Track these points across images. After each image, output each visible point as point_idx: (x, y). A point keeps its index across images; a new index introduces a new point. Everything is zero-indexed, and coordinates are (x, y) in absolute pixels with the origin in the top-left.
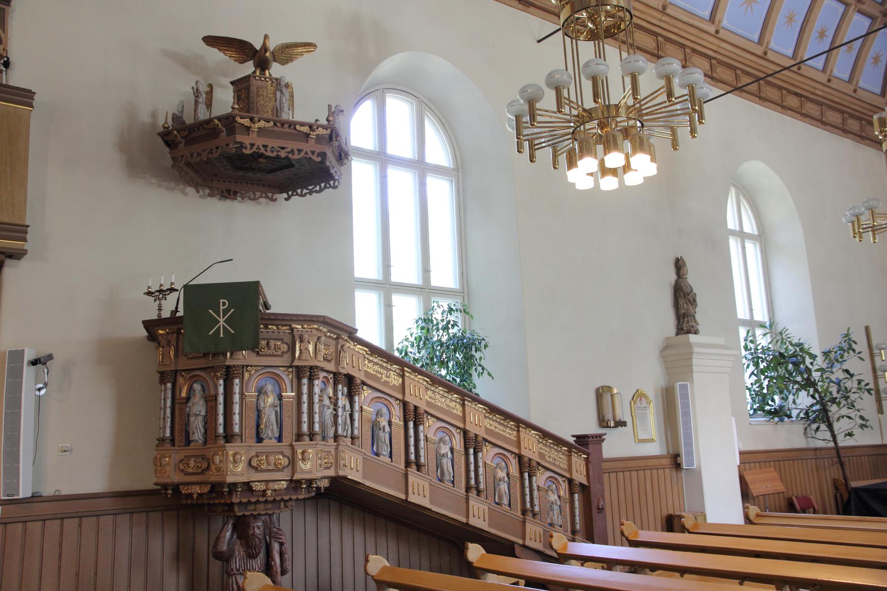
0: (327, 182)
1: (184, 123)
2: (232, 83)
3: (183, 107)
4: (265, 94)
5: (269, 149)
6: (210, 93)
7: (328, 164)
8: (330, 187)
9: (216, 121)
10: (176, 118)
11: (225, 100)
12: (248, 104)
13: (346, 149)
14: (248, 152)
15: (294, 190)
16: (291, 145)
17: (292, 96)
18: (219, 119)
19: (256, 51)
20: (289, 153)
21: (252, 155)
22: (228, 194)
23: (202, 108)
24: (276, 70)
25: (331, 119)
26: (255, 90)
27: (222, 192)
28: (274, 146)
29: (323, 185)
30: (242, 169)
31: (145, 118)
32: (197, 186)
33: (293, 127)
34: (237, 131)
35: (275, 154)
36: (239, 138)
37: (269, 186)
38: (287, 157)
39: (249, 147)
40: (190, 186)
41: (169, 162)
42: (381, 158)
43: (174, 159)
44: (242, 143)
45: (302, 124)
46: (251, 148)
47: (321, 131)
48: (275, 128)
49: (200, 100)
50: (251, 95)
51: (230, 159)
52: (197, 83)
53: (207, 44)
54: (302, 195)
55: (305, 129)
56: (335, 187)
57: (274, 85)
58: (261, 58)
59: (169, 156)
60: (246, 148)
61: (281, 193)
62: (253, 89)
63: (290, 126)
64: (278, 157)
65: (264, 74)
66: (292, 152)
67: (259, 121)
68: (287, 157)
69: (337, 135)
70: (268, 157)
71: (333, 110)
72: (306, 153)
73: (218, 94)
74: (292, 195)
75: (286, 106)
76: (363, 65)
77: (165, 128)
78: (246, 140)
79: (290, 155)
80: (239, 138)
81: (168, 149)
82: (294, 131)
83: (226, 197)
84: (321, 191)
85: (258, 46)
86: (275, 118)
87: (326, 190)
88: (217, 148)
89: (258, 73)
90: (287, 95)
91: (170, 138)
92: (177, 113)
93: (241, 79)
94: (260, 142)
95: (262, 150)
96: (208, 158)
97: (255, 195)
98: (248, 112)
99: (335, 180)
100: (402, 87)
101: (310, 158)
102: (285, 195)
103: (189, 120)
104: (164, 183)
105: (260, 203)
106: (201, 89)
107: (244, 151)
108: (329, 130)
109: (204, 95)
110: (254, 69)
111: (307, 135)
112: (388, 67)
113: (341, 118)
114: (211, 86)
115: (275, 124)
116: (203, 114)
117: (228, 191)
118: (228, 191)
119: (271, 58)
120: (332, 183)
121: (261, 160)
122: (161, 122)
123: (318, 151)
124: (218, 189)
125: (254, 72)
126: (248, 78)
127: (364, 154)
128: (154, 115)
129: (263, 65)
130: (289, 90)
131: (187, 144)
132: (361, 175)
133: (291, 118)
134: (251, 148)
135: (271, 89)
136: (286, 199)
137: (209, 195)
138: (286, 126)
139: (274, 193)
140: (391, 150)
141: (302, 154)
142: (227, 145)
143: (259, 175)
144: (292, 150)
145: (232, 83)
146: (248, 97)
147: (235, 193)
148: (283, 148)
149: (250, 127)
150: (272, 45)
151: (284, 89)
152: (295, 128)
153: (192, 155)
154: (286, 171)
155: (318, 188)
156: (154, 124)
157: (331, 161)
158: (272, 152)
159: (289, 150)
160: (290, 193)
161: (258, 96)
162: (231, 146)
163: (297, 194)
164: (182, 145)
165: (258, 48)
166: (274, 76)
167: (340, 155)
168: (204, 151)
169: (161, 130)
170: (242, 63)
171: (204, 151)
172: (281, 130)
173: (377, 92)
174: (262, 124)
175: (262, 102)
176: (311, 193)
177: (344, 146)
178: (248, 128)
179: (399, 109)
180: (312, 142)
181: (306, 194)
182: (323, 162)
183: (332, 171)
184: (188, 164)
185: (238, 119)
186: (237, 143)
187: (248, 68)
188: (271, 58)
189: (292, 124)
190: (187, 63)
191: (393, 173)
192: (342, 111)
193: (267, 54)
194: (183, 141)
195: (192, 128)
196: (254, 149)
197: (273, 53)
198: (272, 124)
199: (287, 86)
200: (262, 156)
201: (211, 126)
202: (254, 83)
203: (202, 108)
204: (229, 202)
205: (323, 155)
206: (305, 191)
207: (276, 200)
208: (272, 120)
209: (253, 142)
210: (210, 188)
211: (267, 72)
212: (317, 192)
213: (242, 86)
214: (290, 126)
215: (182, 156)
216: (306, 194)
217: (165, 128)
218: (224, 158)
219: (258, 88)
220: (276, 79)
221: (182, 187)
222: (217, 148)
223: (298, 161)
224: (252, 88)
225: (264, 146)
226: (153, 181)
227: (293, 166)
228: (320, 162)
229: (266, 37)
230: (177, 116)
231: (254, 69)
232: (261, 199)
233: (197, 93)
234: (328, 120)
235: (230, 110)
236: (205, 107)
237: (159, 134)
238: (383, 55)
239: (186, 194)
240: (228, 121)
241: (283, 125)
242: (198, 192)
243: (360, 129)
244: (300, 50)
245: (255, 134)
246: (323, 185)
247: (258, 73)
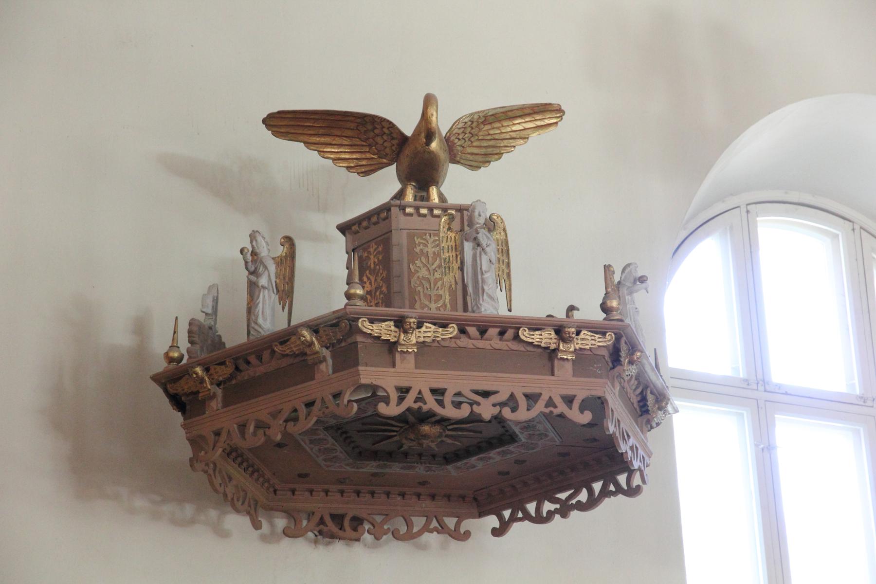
0: (609, 478)
1: (218, 343)
2: (344, 228)
3: (216, 301)
4: (430, 249)
5: (448, 399)
6: (288, 260)
7: (612, 429)
8: (619, 490)
9: (307, 335)
10: (201, 333)
11: (326, 279)
12: (388, 280)
13: (658, 382)
14: (391, 410)
15: (518, 506)
16: (507, 384)
17: (505, 250)
18: (315, 327)
19: (404, 139)
20: (502, 404)
21: (401, 419)
22: (337, 527)
23: (268, 301)
24: (457, 184)
25: (614, 303)
26: (405, 242)
27: (322, 521)
28: (461, 389)
29: (597, 486)
30: (375, 455)
31: (117, 335)
32: (253, 510)
33: (510, 333)
34: (361, 355)
35: (464, 412)
36: (368, 374)
37: (449, 497)
38: (498, 419)
39: (394, 396)
40: (238, 511)
41: (179, 447)
42: (756, 396)
43: (196, 442)
44: (374, 388)
45: (536, 326)
46: (401, 399)
47: (587, 340)
48: (464, 342)
49: (263, 281)
50: (395, 254)
51: (340, 430)
52: (253, 237)
53: (276, 134)
54: (540, 519)
55: (546, 338)
56: (632, 492)
57: (456, 225)
58: (414, 157)
59: (182, 433)
60: (386, 400)
61: (481, 515)
62: (400, 239)
63: (502, 333)
64: (475, 418)
65: (428, 198)
66: (512, 402)
67: (420, 325)
68: (498, 419)
69: (633, 348)
70: (443, 421)
71: (617, 278)
72: (550, 403)
73: (305, 259)
74: (513, 519)
75: (490, 277)
76: (690, 148)
77: (171, 360)
78: (384, 377)
79: (507, 413)
80: (368, 374)
81: (178, 417)
82: (514, 346)
83: (333, 536)
84: (592, 503)
85: (408, 126)
86: (460, 313)
87: (607, 502)
88: (310, 405)
89: (410, 196)
90: (492, 251)
91: (183, 387)
92: (201, 317)
93: (367, 217)
94: (422, 381)
95: (431, 404)
96: (286, 434)
97: (409, 524)
98: (388, 303)
99: (631, 473)
100: (804, 194)
101: (561, 416)
102: (492, 521)
103: (234, 336)
104: (167, 508)
105: (424, 547)
106: (264, 252)
107: (382, 408)
108: (610, 338)
109: (272, 268)
110: (398, 186)
111: (551, 354)
112: (756, 147)
113: (639, 298)
114: (289, 242)
115: (462, 331)
116: (271, 319)
117: (338, 519)
118: (338, 519)
119: (443, 155)
120: (622, 479)
121: (426, 428)
122: (160, 344)
123: (581, 395)
124: (310, 515)
125: (400, 195)
126: (382, 214)
127: (708, 390)
128: (140, 327)
129: (422, 173)
130: (497, 235)
131: (226, 403)
132: (699, 454)
133: (503, 311)
134: (401, 399)
135: (448, 238)
136: (497, 532)
137: (287, 533)
138: (493, 332)
139: (461, 519)
140: (781, 373)
141: (540, 407)
142: (337, 396)
143: (420, 470)
144: (512, 396)
145: (344, 228)
146: (386, 261)
147: (357, 522)
148: (486, 394)
149: (396, 343)
150: (444, 121)
151: (483, 236)
152: (516, 337)
153: (242, 427)
154: (495, 455)
155: (583, 496)
156: (140, 352)
157: (619, 420)
158: (458, 405)
159: (503, 397)
160: (507, 514)
161: (413, 257)
162: (346, 398)
163: (527, 517)
164: (215, 405)
165: (408, 131)
166: (453, 199)
167: (643, 400)
168: (274, 415)
169: (161, 366)
170: (366, 173)
171: (274, 415)
172: (480, 344)
173: (734, 212)
174: (429, 332)
175: (423, 272)
176: (564, 510)
177: (652, 376)
178: (392, 347)
179: (799, 256)
180: (564, 371)
181: (551, 514)
182: (597, 423)
183: (623, 448)
184: (233, 453)
185: (364, 325)
186: (361, 387)
187: (385, 185)
188: (443, 155)
189: (508, 328)
190: (223, 184)
191: (788, 430)
192: (642, 280)
193: (434, 145)
194: (219, 392)
195: (241, 358)
196: (409, 401)
197: (447, 140)
198: (453, 330)
199: (491, 224)
200: (426, 417)
201: (293, 346)
202: (399, 221)
203: (268, 301)
204: (339, 551)
205: (597, 405)
206: (548, 506)
207: (467, 535)
208: (454, 320)
209: (405, 384)
210: (290, 514)
211: (434, 192)
212: (582, 507)
213: (368, 236)
214: (502, 333)
215: (218, 434)
216: (551, 514)
217: (171, 360)
218: (326, 429)
219: (411, 237)
220: (460, 209)
221: (213, 513)
222: (310, 405)
223: (528, 426)
224: (395, 238)
225: (434, 391)
226: (139, 502)
227: (512, 438)
228: (590, 425)
229: (429, 101)
230: (200, 326)
231: (398, 186)
232: (427, 537)
233: (253, 261)
234: (605, 308)
235: (339, 303)
236: (275, 298)
237: (156, 378)
238: (742, 114)
239: (222, 533)
240: (339, 331)
241: (483, 332)
242: (257, 526)
243: (689, 323)
244: (518, 125)
245: (411, 359)
246: (597, 486)
247: (410, 196)
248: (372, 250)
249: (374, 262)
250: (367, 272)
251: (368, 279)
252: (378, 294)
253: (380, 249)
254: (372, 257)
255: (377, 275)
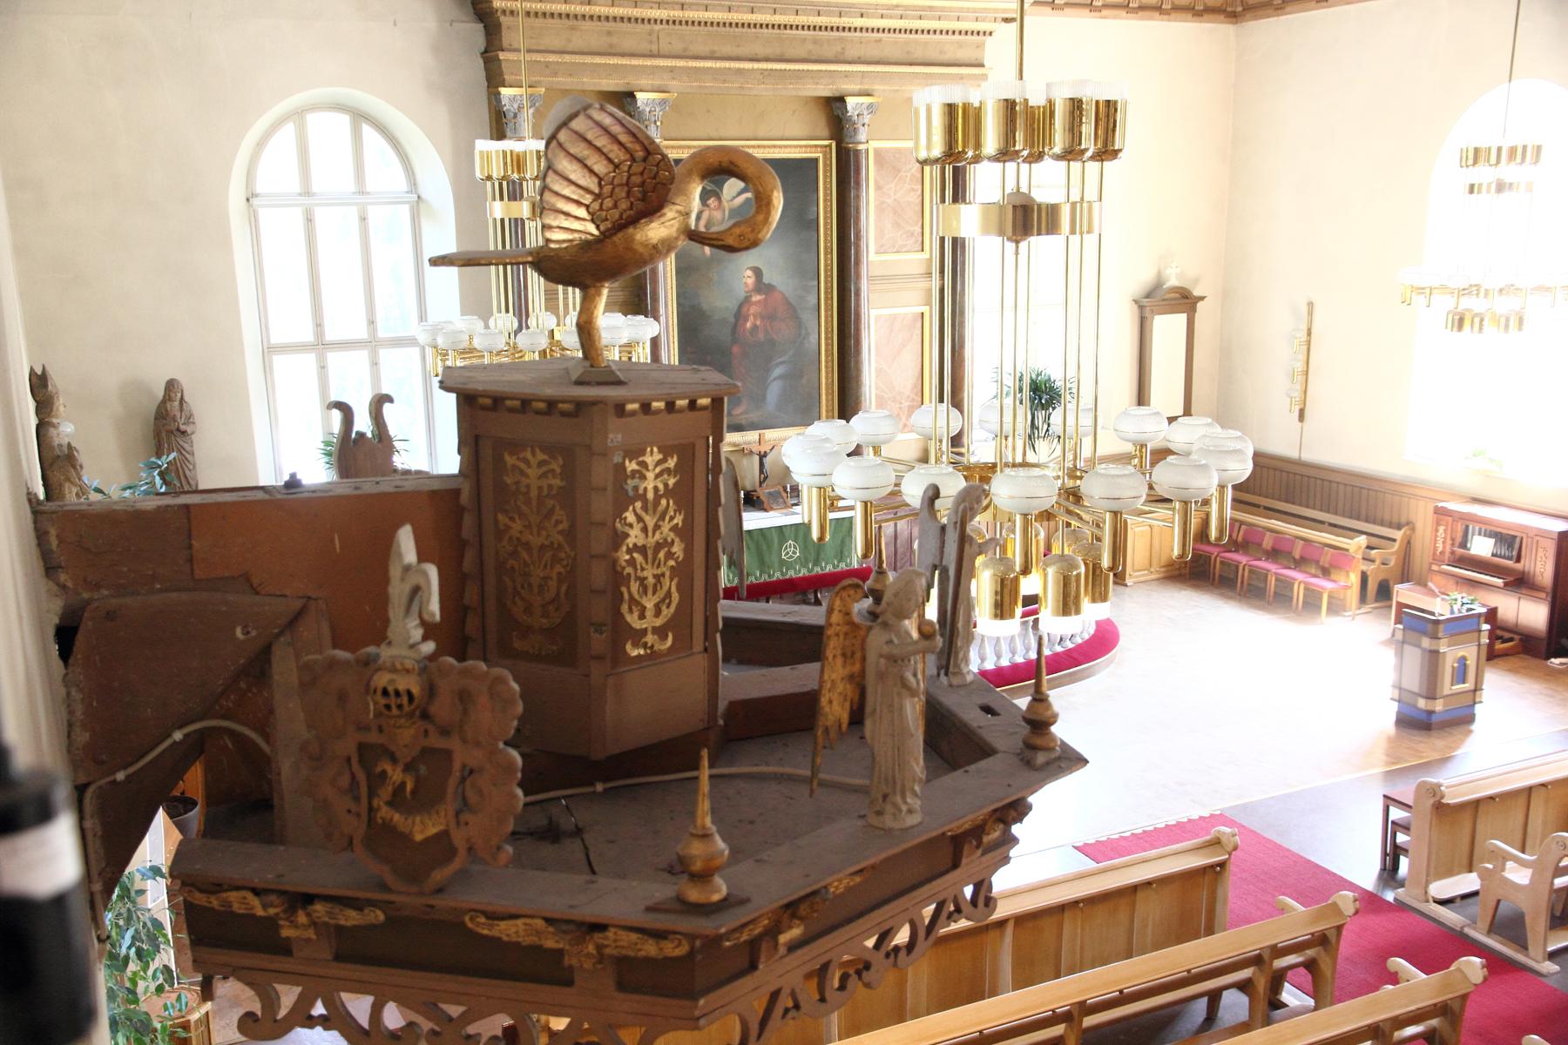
248: (649, 459)
249: (656, 489)
250: (638, 504)
251: (640, 519)
252: (661, 555)
253: (671, 463)
254: (650, 475)
255: (662, 518)
